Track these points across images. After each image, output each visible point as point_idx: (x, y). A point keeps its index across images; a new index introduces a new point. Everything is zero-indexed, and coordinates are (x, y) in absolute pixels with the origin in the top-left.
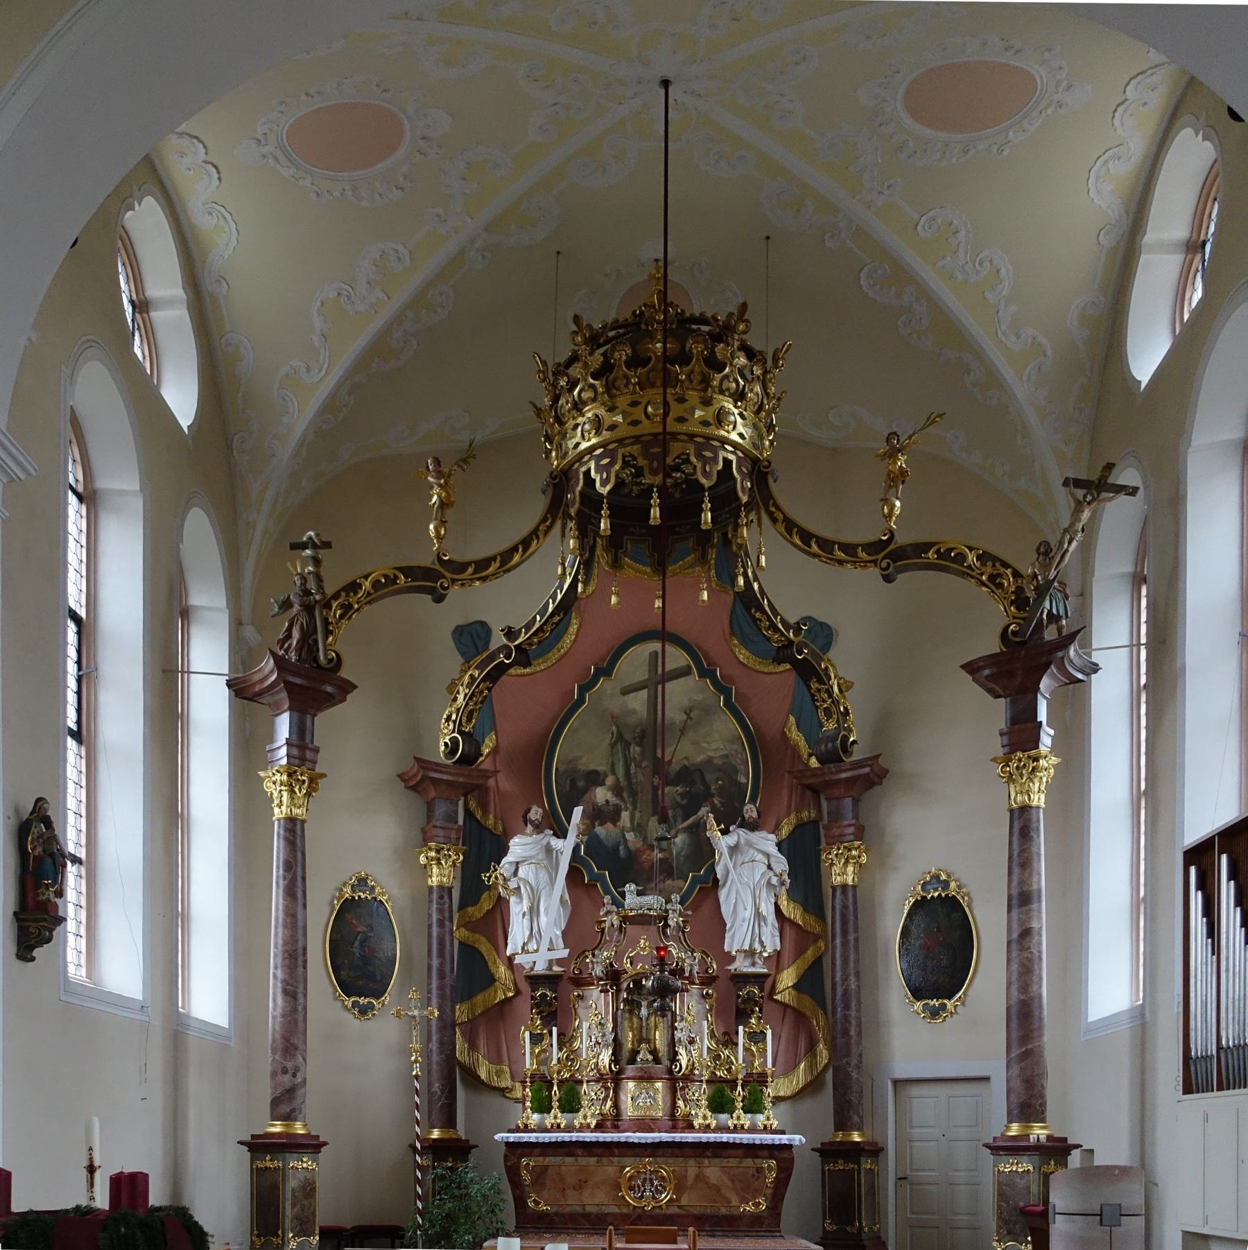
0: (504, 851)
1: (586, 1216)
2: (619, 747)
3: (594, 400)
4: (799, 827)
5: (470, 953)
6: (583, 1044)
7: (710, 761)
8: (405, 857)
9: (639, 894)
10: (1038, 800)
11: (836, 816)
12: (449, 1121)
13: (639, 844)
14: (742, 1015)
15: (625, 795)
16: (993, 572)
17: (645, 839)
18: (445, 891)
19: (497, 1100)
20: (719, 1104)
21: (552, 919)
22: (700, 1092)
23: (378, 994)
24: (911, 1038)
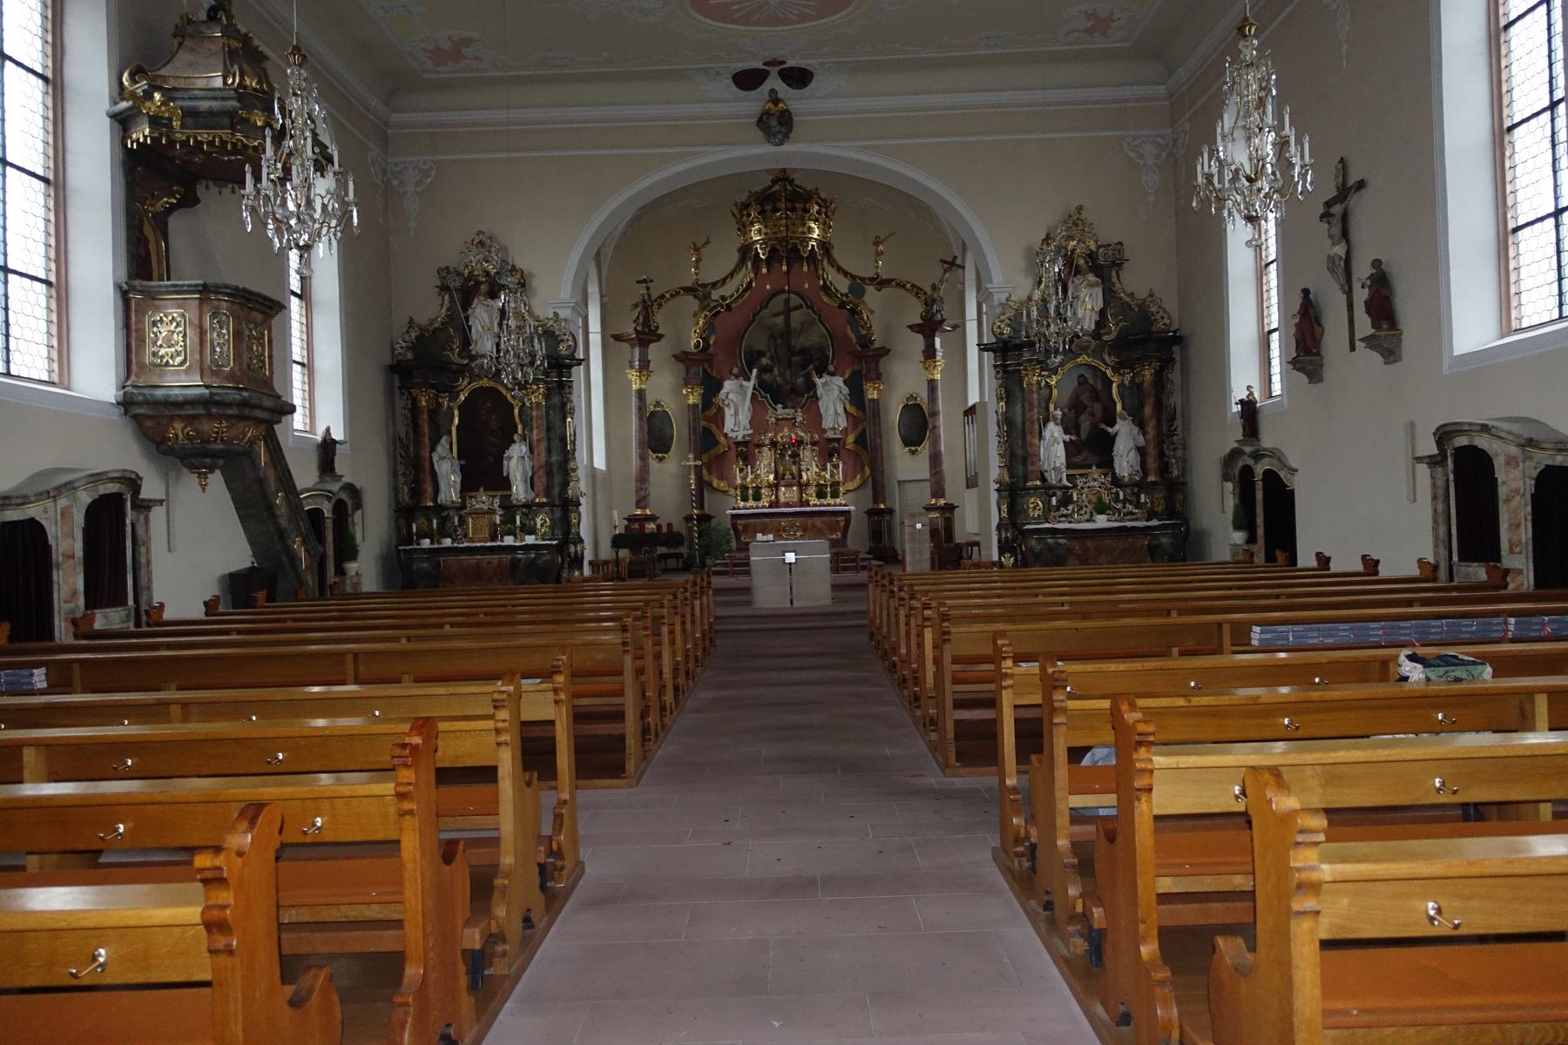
0: (721, 387)
4: (853, 373)
5: (707, 431)
6: (762, 471)
8: (677, 392)
10: (938, 377)
11: (868, 370)
12: (701, 506)
14: (831, 456)
16: (917, 291)
18: (695, 406)
19: (718, 496)
20: (821, 495)
21: (745, 416)
22: (812, 490)
23: (667, 451)
24: (907, 465)
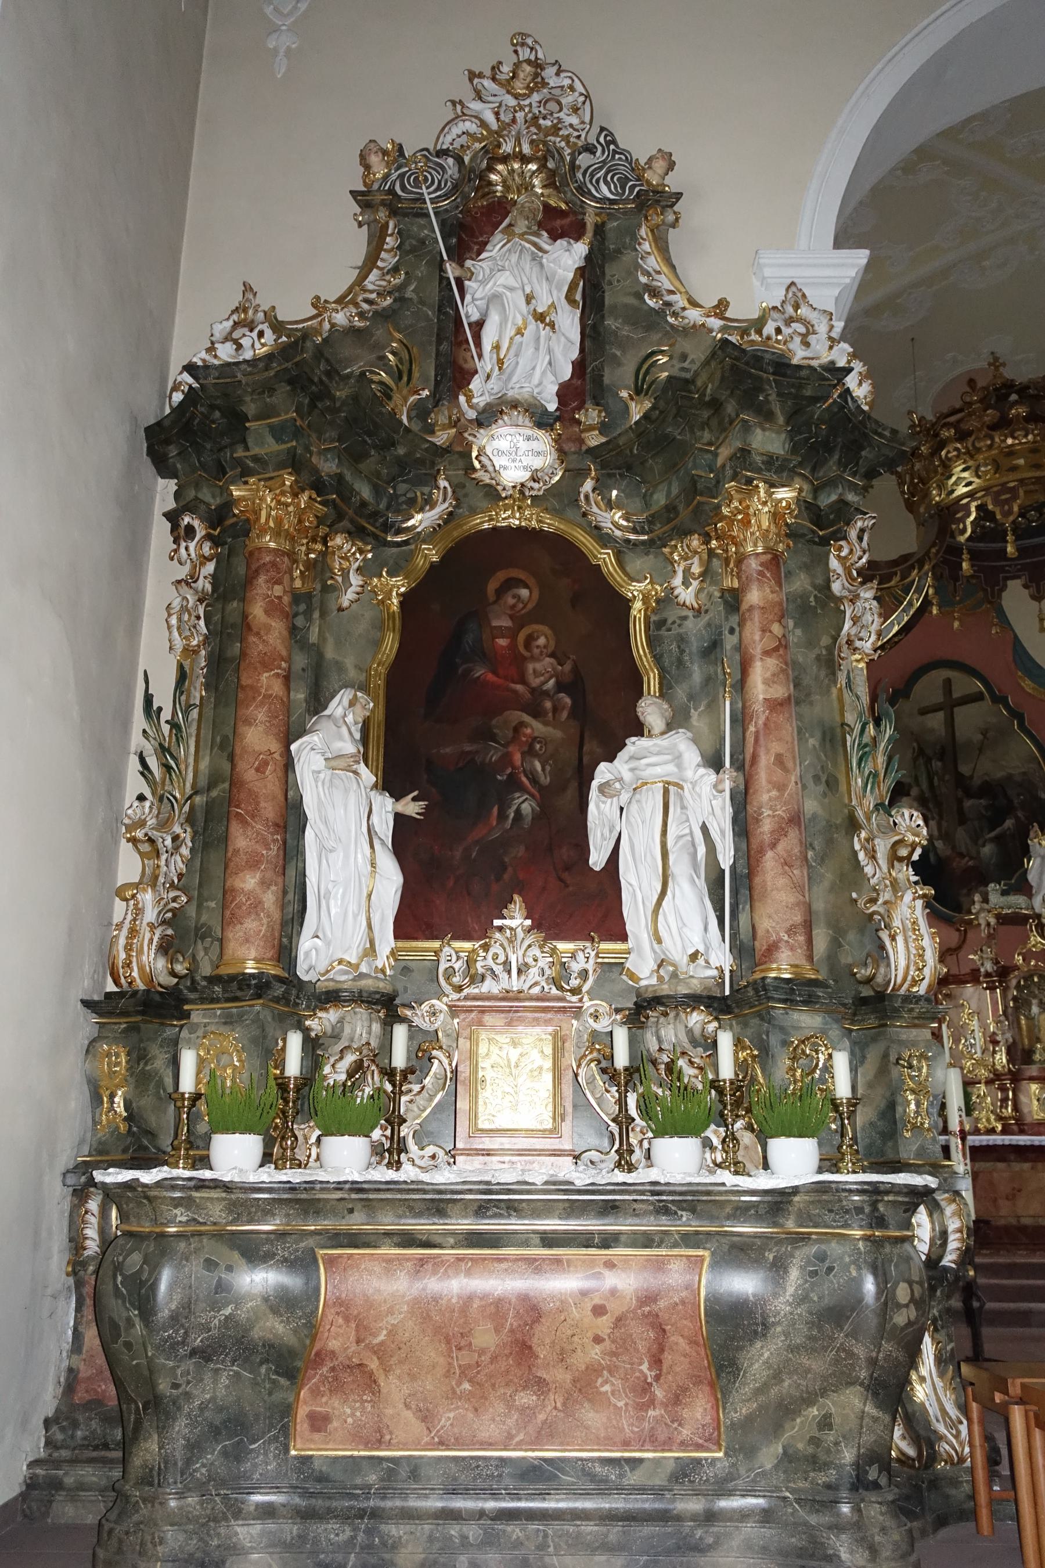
1: (1023, 1229)
2: (921, 761)
3: (958, 457)
7: (1010, 777)
9: (1004, 893)
13: (949, 852)
15: (931, 806)
17: (954, 848)
